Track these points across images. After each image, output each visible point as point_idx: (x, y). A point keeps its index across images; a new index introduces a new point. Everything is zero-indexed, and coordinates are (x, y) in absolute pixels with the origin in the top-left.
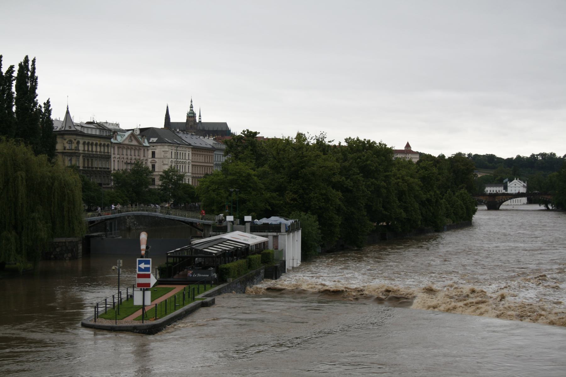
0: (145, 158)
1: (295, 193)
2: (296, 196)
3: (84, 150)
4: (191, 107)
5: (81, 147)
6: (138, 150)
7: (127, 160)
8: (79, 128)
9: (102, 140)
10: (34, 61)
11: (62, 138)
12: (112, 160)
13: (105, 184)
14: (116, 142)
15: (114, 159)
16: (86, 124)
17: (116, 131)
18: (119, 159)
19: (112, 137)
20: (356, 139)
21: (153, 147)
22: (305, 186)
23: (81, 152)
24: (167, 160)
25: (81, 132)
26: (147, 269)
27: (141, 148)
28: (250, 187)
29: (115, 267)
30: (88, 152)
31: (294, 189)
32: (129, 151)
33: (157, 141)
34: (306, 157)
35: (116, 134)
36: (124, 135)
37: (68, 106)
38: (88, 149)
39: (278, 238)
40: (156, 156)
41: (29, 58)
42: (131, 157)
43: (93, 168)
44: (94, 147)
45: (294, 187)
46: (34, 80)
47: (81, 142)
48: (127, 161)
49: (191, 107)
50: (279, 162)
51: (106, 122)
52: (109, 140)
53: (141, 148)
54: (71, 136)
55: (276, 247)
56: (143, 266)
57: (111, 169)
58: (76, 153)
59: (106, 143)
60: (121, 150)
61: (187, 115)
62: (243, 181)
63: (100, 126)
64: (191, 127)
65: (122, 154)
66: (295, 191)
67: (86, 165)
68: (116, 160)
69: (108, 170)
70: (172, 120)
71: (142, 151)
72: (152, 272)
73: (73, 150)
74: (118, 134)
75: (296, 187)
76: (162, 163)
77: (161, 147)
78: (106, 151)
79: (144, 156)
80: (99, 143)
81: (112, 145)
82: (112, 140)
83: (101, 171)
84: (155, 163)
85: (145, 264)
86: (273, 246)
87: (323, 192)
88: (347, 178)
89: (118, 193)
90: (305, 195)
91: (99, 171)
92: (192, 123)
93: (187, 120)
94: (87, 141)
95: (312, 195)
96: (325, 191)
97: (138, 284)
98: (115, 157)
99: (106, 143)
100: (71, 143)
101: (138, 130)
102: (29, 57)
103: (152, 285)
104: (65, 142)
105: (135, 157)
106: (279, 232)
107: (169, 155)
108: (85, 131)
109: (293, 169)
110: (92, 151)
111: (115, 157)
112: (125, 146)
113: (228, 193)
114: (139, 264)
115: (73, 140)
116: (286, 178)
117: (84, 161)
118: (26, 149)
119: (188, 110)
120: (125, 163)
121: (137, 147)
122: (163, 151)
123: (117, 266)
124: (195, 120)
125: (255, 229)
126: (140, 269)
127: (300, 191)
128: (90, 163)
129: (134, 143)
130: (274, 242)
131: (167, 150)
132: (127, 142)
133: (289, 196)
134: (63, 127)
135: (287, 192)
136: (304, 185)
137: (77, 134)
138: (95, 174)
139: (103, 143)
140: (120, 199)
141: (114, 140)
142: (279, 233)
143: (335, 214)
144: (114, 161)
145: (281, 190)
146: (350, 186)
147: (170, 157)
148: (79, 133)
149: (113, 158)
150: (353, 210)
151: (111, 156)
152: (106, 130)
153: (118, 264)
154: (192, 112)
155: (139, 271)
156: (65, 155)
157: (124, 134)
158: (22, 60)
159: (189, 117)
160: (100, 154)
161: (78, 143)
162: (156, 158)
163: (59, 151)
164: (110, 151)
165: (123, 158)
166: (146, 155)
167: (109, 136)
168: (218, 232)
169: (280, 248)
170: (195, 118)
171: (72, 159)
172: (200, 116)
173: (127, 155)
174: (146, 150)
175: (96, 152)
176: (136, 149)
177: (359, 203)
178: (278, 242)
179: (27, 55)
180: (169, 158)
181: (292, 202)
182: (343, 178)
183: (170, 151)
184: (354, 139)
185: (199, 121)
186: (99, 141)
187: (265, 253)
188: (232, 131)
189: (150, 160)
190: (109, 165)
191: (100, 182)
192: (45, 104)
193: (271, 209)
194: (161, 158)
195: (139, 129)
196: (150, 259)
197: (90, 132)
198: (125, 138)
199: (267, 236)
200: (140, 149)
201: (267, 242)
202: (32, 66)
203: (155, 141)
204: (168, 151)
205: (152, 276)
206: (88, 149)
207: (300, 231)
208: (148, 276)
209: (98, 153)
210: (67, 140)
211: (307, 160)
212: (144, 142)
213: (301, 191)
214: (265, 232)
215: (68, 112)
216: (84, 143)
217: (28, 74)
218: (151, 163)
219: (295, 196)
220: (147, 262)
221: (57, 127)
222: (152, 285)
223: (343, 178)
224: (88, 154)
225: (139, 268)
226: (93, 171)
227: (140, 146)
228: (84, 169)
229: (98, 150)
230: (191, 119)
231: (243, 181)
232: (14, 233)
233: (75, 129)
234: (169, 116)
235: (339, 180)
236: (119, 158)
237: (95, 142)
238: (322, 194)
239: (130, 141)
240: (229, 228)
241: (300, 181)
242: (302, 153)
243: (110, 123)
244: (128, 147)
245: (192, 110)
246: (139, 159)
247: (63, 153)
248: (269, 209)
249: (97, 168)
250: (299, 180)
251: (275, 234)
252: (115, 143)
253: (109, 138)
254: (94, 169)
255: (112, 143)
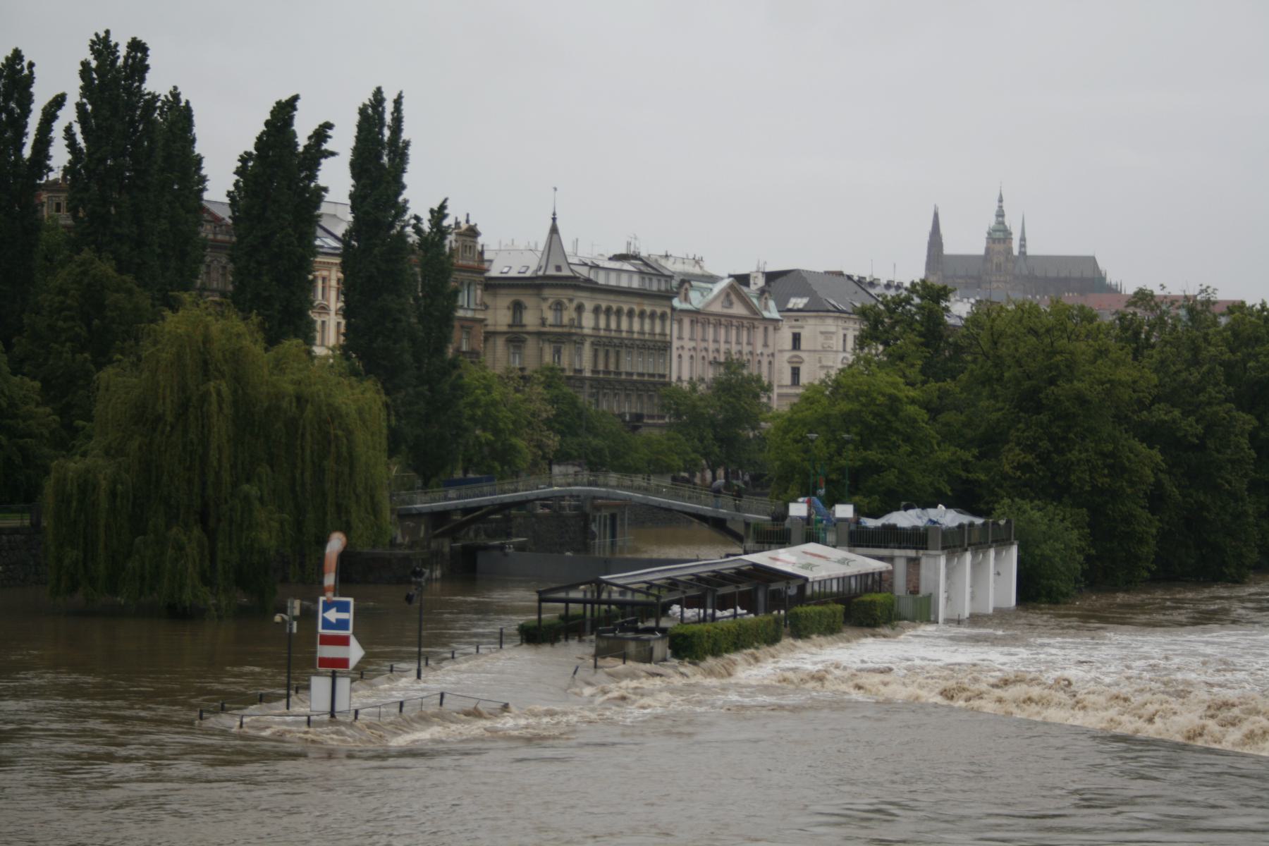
0: (769, 351)
1: (1031, 448)
2: (1029, 458)
3: (596, 328)
4: (1000, 214)
5: (588, 321)
6: (748, 329)
7: (716, 355)
8: (584, 272)
9: (646, 302)
10: (398, 102)
11: (538, 295)
12: (675, 354)
13: (652, 417)
14: (685, 306)
15: (680, 352)
16: (610, 259)
17: (686, 278)
18: (693, 353)
19: (677, 294)
20: (1259, 307)
21: (797, 320)
22: (1057, 430)
23: (587, 331)
24: (831, 356)
25: (588, 280)
26: (342, 624)
27: (756, 323)
28: (897, 432)
29: (283, 619)
30: (607, 334)
31: (1028, 438)
32: (734, 332)
33: (806, 305)
34: (1061, 352)
35: (687, 285)
36: (711, 290)
37: (554, 214)
38: (608, 324)
39: (919, 564)
40: (804, 345)
41: (385, 95)
42: (728, 346)
43: (620, 374)
44: (636, 321)
45: (1026, 434)
46: (400, 153)
47: (589, 305)
48: (715, 358)
49: (1000, 214)
50: (996, 365)
51: (667, 256)
52: (665, 302)
53: (756, 323)
54: (559, 292)
55: (914, 587)
56: (333, 615)
57: (670, 377)
58: (570, 334)
59: (659, 311)
60: (699, 328)
61: (986, 235)
62: (876, 415)
63: (649, 268)
64: (999, 266)
65: (704, 340)
66: (1029, 443)
67: (601, 367)
68: (686, 355)
69: (662, 380)
70: (948, 249)
71: (759, 334)
72: (354, 633)
73: (565, 326)
74: (691, 286)
75: (1032, 433)
76: (819, 365)
77: (818, 321)
78: (658, 330)
79: (766, 345)
80: (637, 309)
81: (676, 316)
82: (676, 303)
83: (643, 383)
84: (801, 363)
85: (338, 611)
86: (907, 584)
87: (1105, 449)
88: (1186, 414)
89: (672, 443)
90: (1054, 456)
91: (636, 381)
92: (1002, 259)
93: (987, 249)
94: (604, 305)
95: (1073, 455)
96: (1111, 447)
97: (320, 658)
98: (682, 347)
99: (659, 311)
100: (561, 310)
101: (760, 275)
102: (383, 90)
103: (352, 663)
104: (545, 306)
105: (739, 348)
106: (922, 549)
107: (836, 343)
108: (601, 279)
109: (1027, 384)
110: (619, 330)
111: (682, 347)
112: (711, 319)
113: (833, 446)
114: (325, 610)
115: (566, 301)
116: (1008, 410)
117: (596, 356)
118: (243, 325)
119: (992, 221)
120: (710, 363)
121: (745, 322)
122: (822, 333)
123: (285, 613)
124: (1010, 250)
125: (858, 539)
126: (327, 625)
127: (1040, 444)
128: (612, 360)
129: (738, 309)
130: (908, 574)
131: (833, 329)
132: (717, 308)
133: (1011, 457)
134: (541, 268)
135: (1007, 447)
136: (1055, 430)
137: (575, 285)
138: (626, 389)
139: (648, 309)
140: (676, 457)
141: (681, 302)
142: (921, 552)
143: (1143, 507)
144: (680, 356)
145: (990, 443)
146: (1192, 435)
147: (841, 348)
148: (582, 284)
149: (678, 349)
150: (1202, 499)
151: (671, 343)
152: (663, 275)
153: (289, 611)
154: (1001, 227)
155: (323, 628)
156: (543, 341)
157: (710, 286)
158: (366, 97)
159: (994, 242)
160: (642, 337)
161: (580, 309)
162: (805, 351)
163: (529, 329)
164: (668, 332)
165: (706, 350)
166: (770, 342)
167: (667, 291)
168: (767, 543)
169: (923, 591)
170: (1011, 243)
171: (562, 350)
172: (1023, 239)
173: (716, 341)
174: (771, 328)
175: (630, 331)
176: (743, 326)
177: (1219, 481)
178: (918, 574)
179: (378, 85)
180: (837, 352)
181: (1019, 473)
182: (1177, 413)
183: (841, 333)
184: (1253, 306)
185: (1020, 252)
186: (638, 304)
187: (863, 601)
188: (1112, 278)
189: (787, 355)
190: (665, 369)
191: (639, 411)
192: (432, 211)
193: (950, 493)
194: (815, 351)
195: (763, 273)
196: (351, 600)
197: (613, 281)
198: (711, 296)
199: (890, 559)
200: (754, 327)
201: (891, 573)
202: (392, 114)
203: (801, 306)
204: (833, 333)
205: (353, 641)
206: (608, 324)
207: (1014, 551)
208: (344, 641)
209: (636, 336)
210: (550, 301)
211: (1062, 361)
212: (766, 308)
213: (1045, 444)
214: (886, 547)
215: (554, 230)
216: (597, 310)
217: (383, 135)
218: (789, 362)
219: (1029, 458)
220: (343, 607)
221: (528, 267)
222: (352, 663)
223: (1177, 413)
224: (607, 337)
225: (325, 620)
226: (620, 382)
227: (754, 320)
228: (595, 376)
229: (636, 327)
230: (999, 247)
231: (876, 415)
232: (197, 531)
233: (570, 274)
234: (941, 239)
235: (1163, 416)
236: (694, 349)
237: (626, 308)
238: (1103, 455)
239: (726, 304)
240: (794, 536)
241: (1044, 417)
242: (1052, 343)
243: (676, 258)
244: (721, 321)
245: (1003, 223)
246: (751, 353)
247: (539, 335)
248: (946, 494)
249: (631, 374)
250: (1041, 416)
251: (911, 553)
252: (682, 311)
253: (667, 296)
254: (623, 377)
255: (673, 309)
